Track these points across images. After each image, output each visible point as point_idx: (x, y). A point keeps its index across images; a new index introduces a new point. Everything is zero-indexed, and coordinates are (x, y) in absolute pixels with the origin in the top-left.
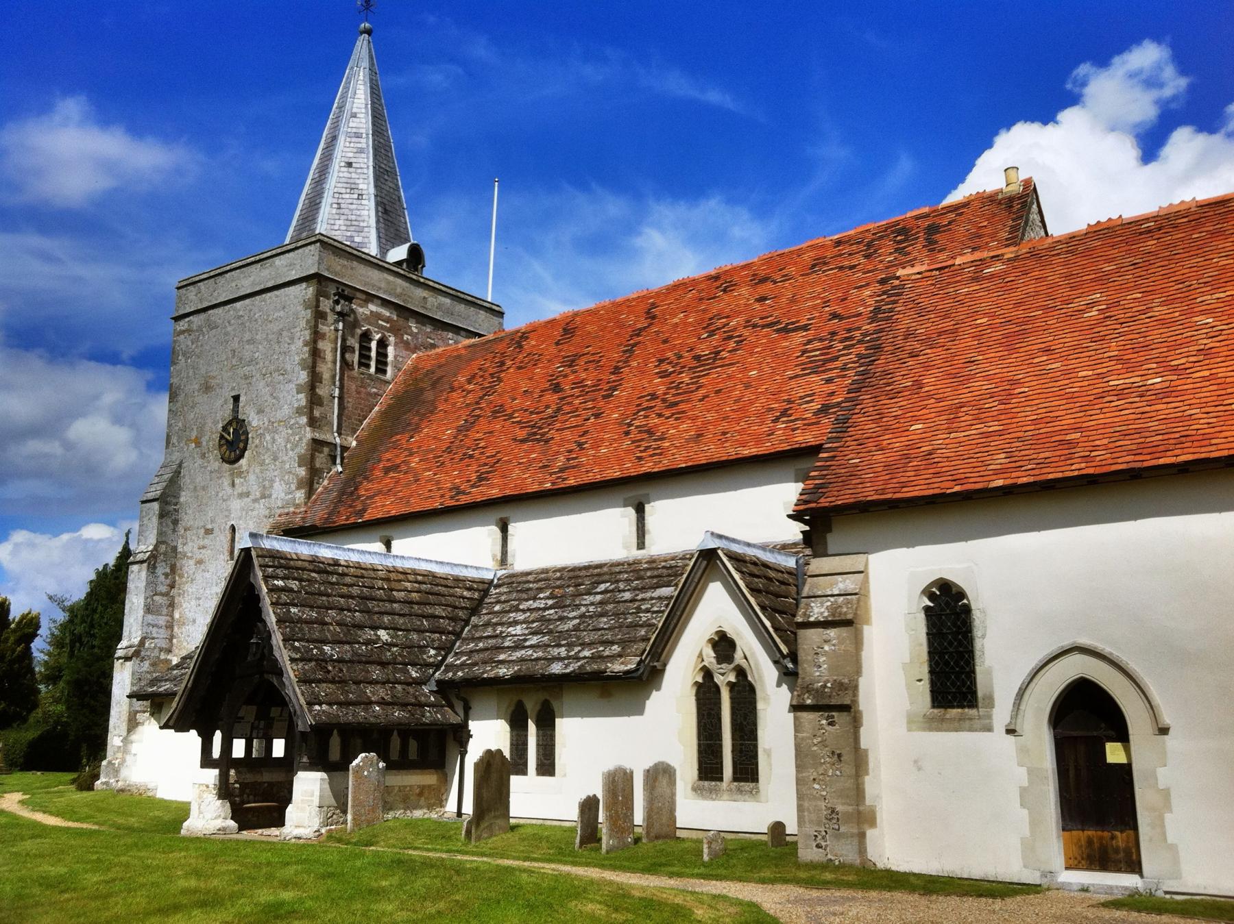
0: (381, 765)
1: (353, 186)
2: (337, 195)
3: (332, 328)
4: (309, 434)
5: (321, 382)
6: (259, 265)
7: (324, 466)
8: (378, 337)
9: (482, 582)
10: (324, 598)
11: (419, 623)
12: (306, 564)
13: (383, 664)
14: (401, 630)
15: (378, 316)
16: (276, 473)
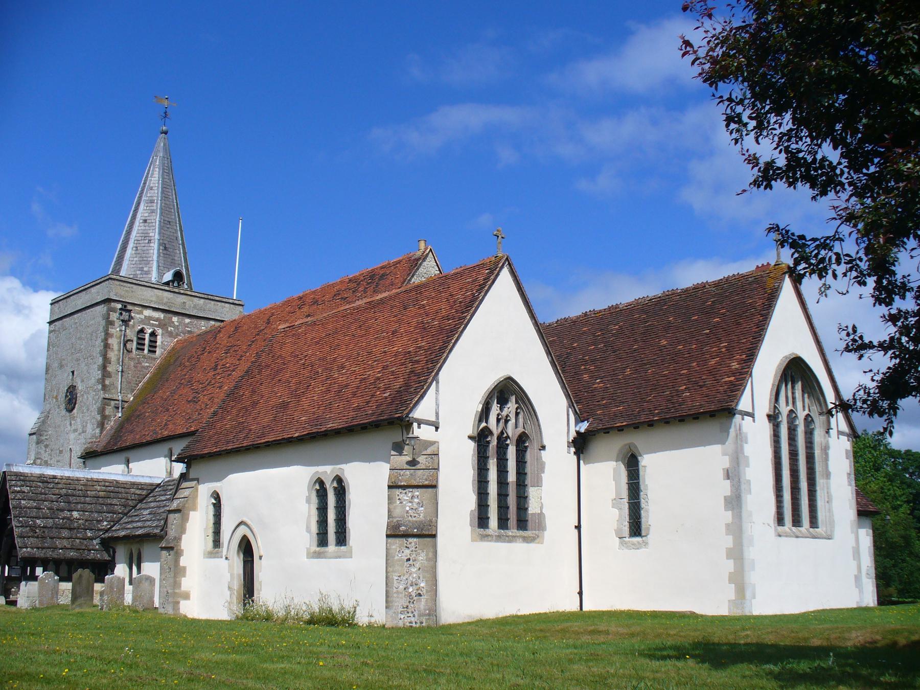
0: (56, 578)
1: (146, 235)
2: (136, 242)
3: (118, 329)
4: (102, 394)
5: (110, 363)
6: (84, 292)
7: (112, 413)
8: (150, 331)
9: (151, 485)
10: (43, 496)
11: (100, 508)
12: (36, 479)
13: (70, 529)
14: (87, 512)
15: (150, 318)
16: (88, 418)
